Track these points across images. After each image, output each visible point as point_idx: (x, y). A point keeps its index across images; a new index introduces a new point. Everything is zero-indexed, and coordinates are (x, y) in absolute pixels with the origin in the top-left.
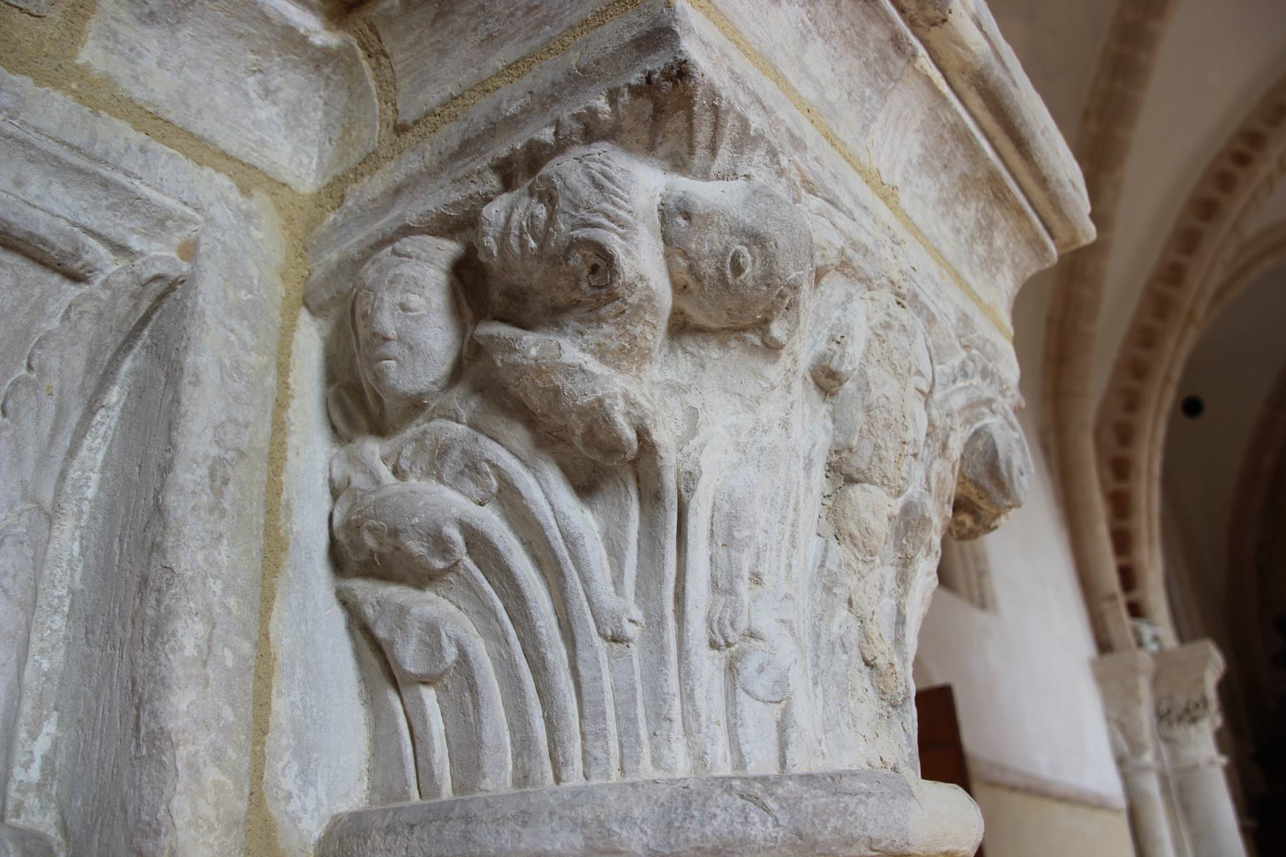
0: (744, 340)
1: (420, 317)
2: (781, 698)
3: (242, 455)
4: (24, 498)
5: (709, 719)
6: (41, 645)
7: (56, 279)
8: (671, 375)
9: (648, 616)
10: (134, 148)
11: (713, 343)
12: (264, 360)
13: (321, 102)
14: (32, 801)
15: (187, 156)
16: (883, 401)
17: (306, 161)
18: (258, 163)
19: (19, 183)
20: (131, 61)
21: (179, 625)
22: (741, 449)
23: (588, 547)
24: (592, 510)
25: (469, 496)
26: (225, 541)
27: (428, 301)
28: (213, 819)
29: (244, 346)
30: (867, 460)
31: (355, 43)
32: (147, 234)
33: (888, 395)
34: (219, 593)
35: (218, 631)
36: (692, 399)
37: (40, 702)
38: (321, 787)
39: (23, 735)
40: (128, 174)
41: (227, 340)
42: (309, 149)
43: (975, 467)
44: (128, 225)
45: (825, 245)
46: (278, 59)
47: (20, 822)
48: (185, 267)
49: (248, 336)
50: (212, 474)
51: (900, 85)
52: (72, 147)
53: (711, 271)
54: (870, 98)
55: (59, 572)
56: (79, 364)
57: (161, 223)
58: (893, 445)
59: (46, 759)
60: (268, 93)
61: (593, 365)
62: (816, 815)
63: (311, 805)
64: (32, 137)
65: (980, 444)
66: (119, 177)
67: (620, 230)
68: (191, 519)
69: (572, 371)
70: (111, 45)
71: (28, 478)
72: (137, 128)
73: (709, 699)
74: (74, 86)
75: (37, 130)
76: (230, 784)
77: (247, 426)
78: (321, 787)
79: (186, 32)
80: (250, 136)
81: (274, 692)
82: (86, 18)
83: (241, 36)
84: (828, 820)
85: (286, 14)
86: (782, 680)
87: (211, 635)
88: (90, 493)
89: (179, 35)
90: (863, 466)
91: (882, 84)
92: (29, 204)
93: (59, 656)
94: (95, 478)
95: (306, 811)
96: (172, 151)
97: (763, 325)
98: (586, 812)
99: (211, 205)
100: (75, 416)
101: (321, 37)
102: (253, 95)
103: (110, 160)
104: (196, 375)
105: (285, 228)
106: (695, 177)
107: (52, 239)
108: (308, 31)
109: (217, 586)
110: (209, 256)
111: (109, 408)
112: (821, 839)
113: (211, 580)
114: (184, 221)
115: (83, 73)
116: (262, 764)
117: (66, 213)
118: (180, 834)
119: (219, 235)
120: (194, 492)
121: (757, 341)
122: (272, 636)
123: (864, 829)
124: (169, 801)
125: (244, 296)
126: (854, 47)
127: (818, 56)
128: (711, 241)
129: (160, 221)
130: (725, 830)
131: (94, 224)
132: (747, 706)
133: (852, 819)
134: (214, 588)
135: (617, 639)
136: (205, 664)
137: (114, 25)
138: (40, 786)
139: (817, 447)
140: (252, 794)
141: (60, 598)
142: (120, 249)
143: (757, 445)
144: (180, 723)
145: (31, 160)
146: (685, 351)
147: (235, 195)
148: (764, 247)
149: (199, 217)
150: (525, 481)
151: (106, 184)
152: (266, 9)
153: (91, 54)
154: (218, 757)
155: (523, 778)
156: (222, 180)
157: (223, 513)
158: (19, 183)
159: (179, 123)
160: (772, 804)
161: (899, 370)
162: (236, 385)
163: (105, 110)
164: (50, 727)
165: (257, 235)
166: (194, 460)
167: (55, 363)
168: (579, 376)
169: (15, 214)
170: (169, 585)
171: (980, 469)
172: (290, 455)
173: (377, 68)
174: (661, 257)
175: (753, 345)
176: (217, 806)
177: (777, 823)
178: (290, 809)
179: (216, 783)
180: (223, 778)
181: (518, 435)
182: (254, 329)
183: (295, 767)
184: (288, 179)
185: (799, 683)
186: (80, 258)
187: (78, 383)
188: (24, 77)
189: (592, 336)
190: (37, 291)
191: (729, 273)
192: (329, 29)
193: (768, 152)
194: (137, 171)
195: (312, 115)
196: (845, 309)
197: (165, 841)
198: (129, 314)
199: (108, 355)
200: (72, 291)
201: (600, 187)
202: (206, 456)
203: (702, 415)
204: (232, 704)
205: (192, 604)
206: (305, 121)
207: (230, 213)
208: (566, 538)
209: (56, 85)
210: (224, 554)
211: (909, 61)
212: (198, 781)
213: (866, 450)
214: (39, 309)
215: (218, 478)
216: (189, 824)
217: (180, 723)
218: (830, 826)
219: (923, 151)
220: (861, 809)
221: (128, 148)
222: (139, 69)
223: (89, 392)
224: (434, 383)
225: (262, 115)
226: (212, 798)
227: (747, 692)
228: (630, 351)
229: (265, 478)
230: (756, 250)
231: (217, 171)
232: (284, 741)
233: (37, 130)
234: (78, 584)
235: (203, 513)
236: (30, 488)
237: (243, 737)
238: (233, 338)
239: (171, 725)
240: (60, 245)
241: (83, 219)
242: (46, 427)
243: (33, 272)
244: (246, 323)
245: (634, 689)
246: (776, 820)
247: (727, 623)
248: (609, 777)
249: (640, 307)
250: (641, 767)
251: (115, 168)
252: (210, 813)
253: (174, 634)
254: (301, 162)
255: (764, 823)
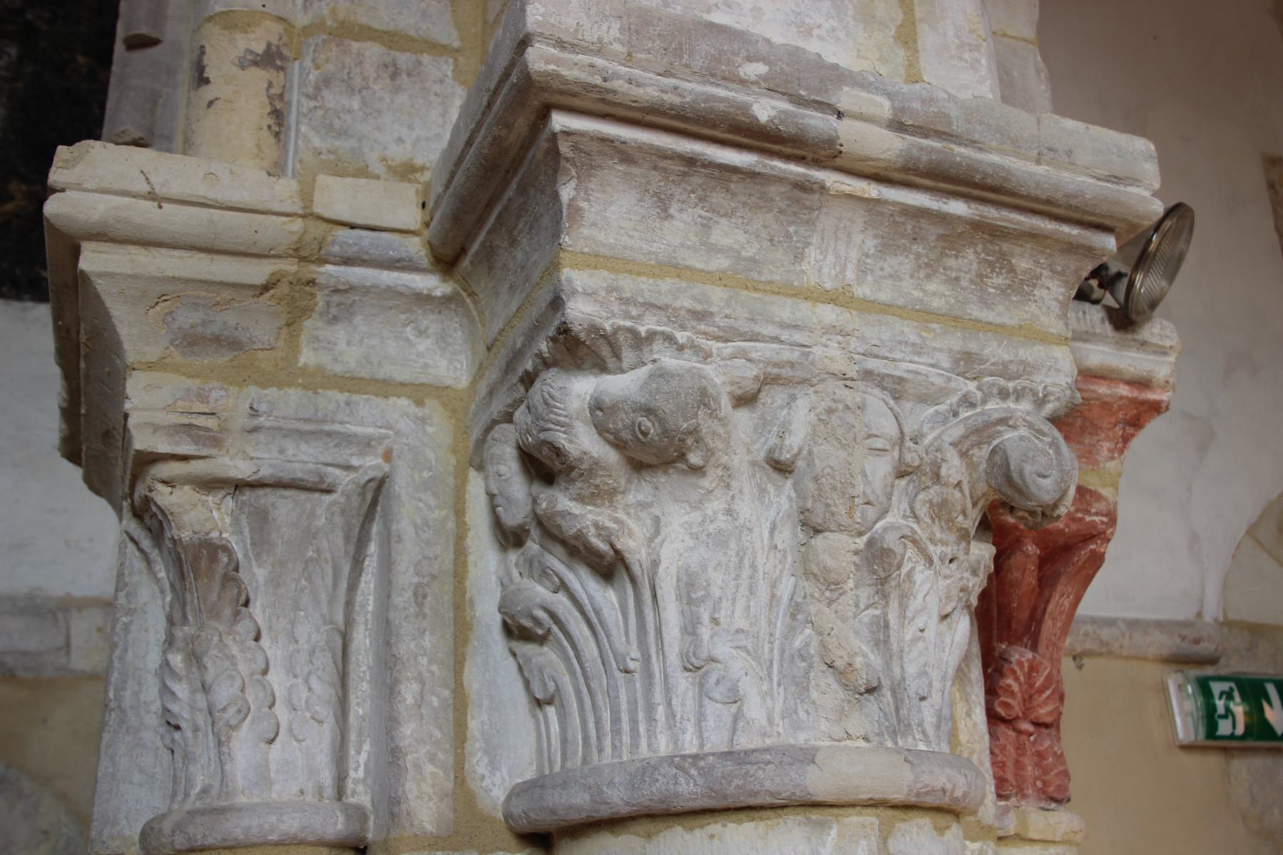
0: (675, 468)
1: (507, 479)
2: (735, 698)
3: (434, 577)
4: (325, 624)
5: (682, 717)
6: (357, 701)
7: (317, 495)
8: (640, 497)
9: (642, 655)
10: (342, 405)
11: (660, 473)
12: (444, 513)
13: (457, 325)
14: (360, 788)
15: (377, 395)
16: (828, 470)
17: (459, 366)
18: (425, 381)
19: (282, 451)
20: (330, 350)
21: (402, 687)
22: (695, 537)
23: (606, 615)
24: (614, 589)
25: (547, 588)
26: (427, 633)
27: (510, 468)
28: (431, 794)
29: (430, 508)
30: (821, 516)
31: (459, 289)
32: (362, 454)
33: (831, 464)
34: (426, 664)
35: (427, 686)
36: (656, 511)
37: (360, 734)
38: (504, 770)
39: (352, 752)
40: (341, 423)
41: (418, 508)
42: (459, 357)
43: (996, 478)
44: (349, 452)
45: (738, 380)
46: (419, 311)
47: (352, 800)
48: (387, 468)
49: (432, 501)
50: (415, 594)
51: (825, 210)
52: (305, 420)
53: (629, 437)
54: (796, 232)
55: (360, 657)
56: (339, 541)
57: (368, 444)
58: (841, 501)
59: (366, 765)
60: (421, 333)
61: (575, 508)
62: (723, 777)
63: (498, 781)
64: (282, 423)
65: (997, 458)
66: (337, 427)
67: (563, 429)
68: (404, 624)
69: (566, 514)
70: (316, 346)
71: (325, 611)
72: (341, 391)
73: (683, 705)
74: (300, 381)
75: (284, 418)
76: (441, 773)
77: (436, 558)
78: (504, 770)
79: (358, 319)
80: (417, 365)
81: (469, 717)
82: (298, 336)
83: (391, 308)
84: (732, 781)
85: (413, 285)
86: (734, 689)
87: (422, 691)
88: (370, 608)
89: (355, 322)
90: (820, 521)
91: (806, 217)
92: (289, 461)
93: (368, 706)
94: (371, 598)
95: (495, 785)
96: (365, 396)
97: (682, 457)
98: (591, 781)
99: (397, 422)
100: (346, 569)
101: (440, 289)
102: (412, 338)
103: (328, 419)
104: (399, 536)
105: (451, 417)
106: (615, 373)
107: (306, 477)
108: (429, 290)
109: (424, 661)
110: (399, 457)
111: (372, 556)
112: (728, 792)
113: (420, 658)
114: (381, 439)
115: (304, 371)
116: (463, 761)
117: (311, 459)
118: (411, 803)
119: (404, 441)
120: (405, 608)
121: (685, 467)
122: (465, 684)
123: (762, 785)
124: (403, 786)
125: (426, 474)
126: (761, 207)
127: (726, 234)
128: (622, 420)
129: (366, 444)
130: (663, 788)
131: (328, 459)
132: (711, 709)
133: (752, 779)
134: (422, 662)
135: (627, 671)
136: (420, 707)
137: (316, 333)
138: (364, 780)
139: (781, 514)
140: (456, 777)
141: (364, 672)
142: (348, 468)
143: (705, 532)
144: (407, 742)
145: (285, 436)
146: (645, 481)
147: (413, 409)
148: (656, 415)
149: (391, 433)
150: (570, 578)
151: (329, 434)
152: (399, 289)
153: (307, 357)
154: (432, 759)
155: (585, 760)
156: (404, 402)
157: (425, 616)
158: (282, 451)
159: (367, 377)
160: (693, 772)
161: (844, 442)
162: (426, 535)
163: (321, 388)
164: (366, 747)
165: (430, 430)
166: (403, 589)
167: (325, 544)
168: (568, 517)
169: (282, 471)
170: (395, 665)
171: (1000, 479)
172: (471, 568)
173: (475, 302)
174: (597, 436)
175: (683, 470)
176: (433, 786)
177: (696, 785)
178: (484, 785)
179: (431, 773)
180: (437, 771)
181: (559, 549)
182: (435, 495)
183: (486, 760)
184: (449, 382)
185: (749, 688)
186: (324, 482)
187: (343, 550)
188: (271, 389)
189: (573, 490)
190: (308, 505)
191: (640, 436)
192: (445, 281)
193: (665, 340)
194: (346, 419)
195: (455, 335)
196: (790, 408)
197: (404, 807)
198: (360, 506)
199: (357, 530)
200: (328, 498)
201: (546, 403)
202: (410, 584)
203: (663, 520)
204: (440, 728)
205: (409, 674)
206: (452, 341)
207: (410, 423)
208: (594, 610)
209: (290, 385)
210: (427, 641)
211: (821, 193)
212: (420, 773)
213: (820, 508)
214: (312, 515)
215: (419, 595)
216: (417, 797)
217: (407, 742)
218: (733, 785)
219: (880, 241)
220: (760, 772)
221: (338, 407)
222: (336, 353)
223: (352, 553)
224: (526, 517)
225: (422, 348)
226: (430, 781)
227: (710, 698)
228: (599, 494)
229: (452, 588)
230: (652, 417)
231: (399, 396)
232: (477, 745)
233: (284, 418)
234: (371, 664)
235: (411, 619)
236: (327, 617)
237: (448, 746)
238: (421, 505)
239: (402, 744)
240: (311, 479)
241: (322, 459)
242: (329, 580)
243: (303, 496)
244: (429, 492)
245: (636, 702)
246: (695, 781)
247: (691, 654)
248: (621, 758)
249: (591, 469)
250: (640, 750)
251: (333, 422)
252: (430, 791)
253: (399, 693)
254: (456, 369)
255: (688, 784)
